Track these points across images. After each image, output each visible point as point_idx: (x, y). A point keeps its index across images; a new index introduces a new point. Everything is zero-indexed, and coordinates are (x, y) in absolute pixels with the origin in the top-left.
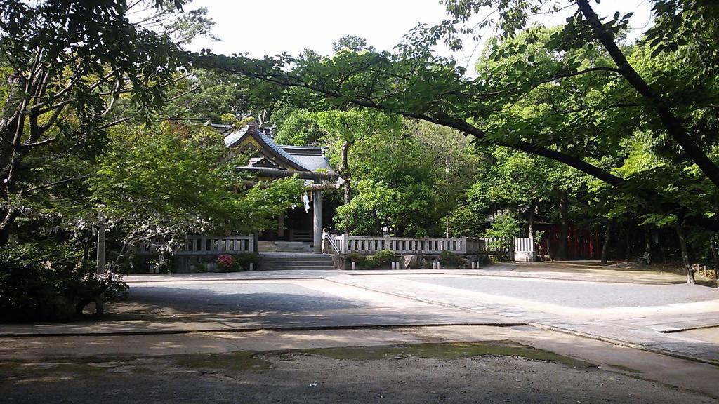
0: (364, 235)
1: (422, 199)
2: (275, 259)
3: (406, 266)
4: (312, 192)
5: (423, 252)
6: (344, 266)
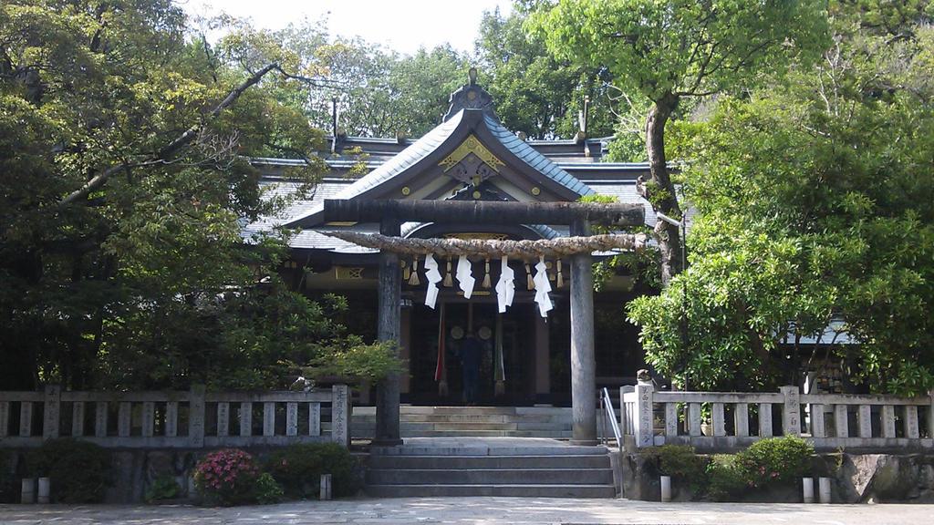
0: (722, 386)
1: (906, 264)
2: (426, 463)
3: (860, 489)
4: (564, 263)
5: (903, 442)
6: (637, 487)
